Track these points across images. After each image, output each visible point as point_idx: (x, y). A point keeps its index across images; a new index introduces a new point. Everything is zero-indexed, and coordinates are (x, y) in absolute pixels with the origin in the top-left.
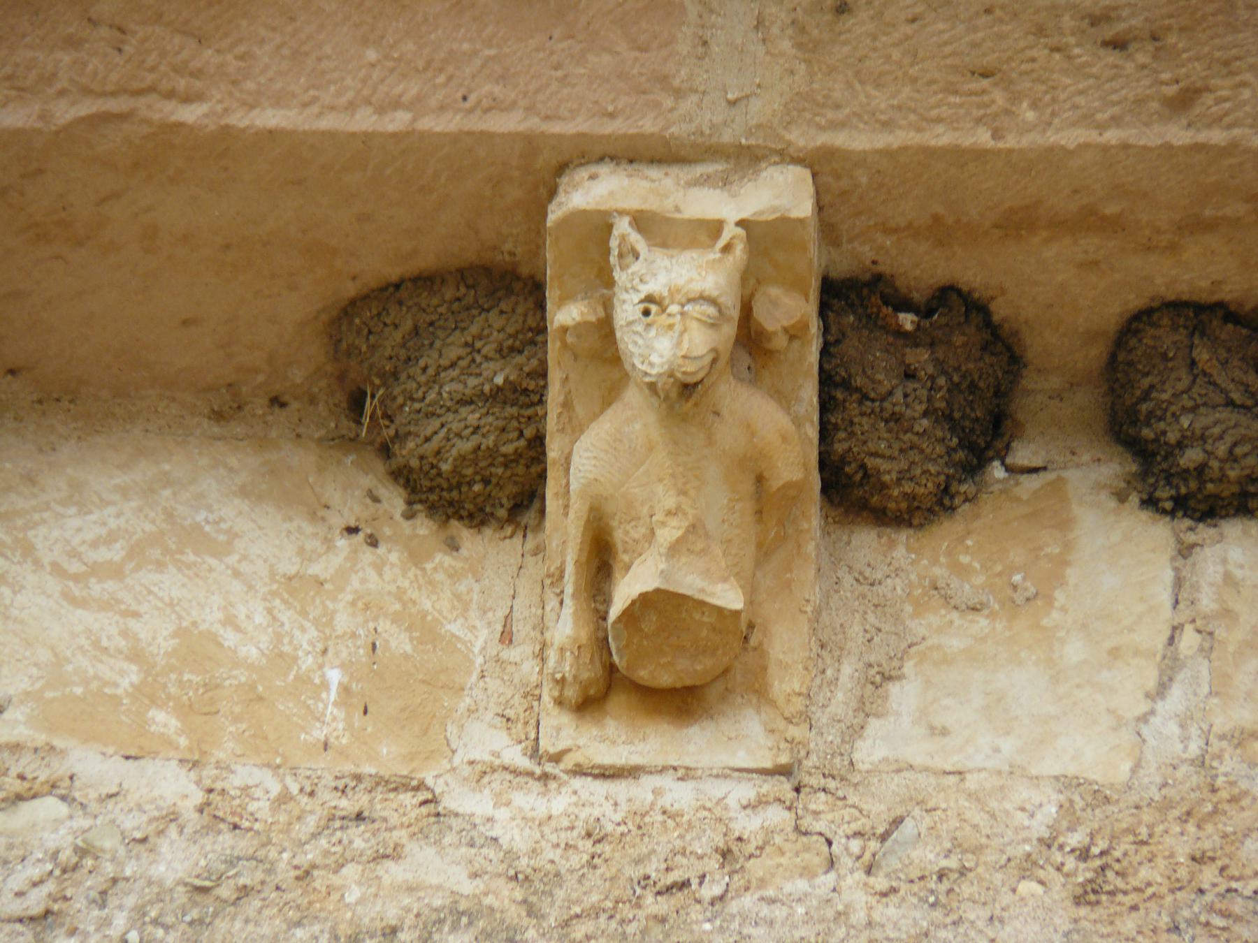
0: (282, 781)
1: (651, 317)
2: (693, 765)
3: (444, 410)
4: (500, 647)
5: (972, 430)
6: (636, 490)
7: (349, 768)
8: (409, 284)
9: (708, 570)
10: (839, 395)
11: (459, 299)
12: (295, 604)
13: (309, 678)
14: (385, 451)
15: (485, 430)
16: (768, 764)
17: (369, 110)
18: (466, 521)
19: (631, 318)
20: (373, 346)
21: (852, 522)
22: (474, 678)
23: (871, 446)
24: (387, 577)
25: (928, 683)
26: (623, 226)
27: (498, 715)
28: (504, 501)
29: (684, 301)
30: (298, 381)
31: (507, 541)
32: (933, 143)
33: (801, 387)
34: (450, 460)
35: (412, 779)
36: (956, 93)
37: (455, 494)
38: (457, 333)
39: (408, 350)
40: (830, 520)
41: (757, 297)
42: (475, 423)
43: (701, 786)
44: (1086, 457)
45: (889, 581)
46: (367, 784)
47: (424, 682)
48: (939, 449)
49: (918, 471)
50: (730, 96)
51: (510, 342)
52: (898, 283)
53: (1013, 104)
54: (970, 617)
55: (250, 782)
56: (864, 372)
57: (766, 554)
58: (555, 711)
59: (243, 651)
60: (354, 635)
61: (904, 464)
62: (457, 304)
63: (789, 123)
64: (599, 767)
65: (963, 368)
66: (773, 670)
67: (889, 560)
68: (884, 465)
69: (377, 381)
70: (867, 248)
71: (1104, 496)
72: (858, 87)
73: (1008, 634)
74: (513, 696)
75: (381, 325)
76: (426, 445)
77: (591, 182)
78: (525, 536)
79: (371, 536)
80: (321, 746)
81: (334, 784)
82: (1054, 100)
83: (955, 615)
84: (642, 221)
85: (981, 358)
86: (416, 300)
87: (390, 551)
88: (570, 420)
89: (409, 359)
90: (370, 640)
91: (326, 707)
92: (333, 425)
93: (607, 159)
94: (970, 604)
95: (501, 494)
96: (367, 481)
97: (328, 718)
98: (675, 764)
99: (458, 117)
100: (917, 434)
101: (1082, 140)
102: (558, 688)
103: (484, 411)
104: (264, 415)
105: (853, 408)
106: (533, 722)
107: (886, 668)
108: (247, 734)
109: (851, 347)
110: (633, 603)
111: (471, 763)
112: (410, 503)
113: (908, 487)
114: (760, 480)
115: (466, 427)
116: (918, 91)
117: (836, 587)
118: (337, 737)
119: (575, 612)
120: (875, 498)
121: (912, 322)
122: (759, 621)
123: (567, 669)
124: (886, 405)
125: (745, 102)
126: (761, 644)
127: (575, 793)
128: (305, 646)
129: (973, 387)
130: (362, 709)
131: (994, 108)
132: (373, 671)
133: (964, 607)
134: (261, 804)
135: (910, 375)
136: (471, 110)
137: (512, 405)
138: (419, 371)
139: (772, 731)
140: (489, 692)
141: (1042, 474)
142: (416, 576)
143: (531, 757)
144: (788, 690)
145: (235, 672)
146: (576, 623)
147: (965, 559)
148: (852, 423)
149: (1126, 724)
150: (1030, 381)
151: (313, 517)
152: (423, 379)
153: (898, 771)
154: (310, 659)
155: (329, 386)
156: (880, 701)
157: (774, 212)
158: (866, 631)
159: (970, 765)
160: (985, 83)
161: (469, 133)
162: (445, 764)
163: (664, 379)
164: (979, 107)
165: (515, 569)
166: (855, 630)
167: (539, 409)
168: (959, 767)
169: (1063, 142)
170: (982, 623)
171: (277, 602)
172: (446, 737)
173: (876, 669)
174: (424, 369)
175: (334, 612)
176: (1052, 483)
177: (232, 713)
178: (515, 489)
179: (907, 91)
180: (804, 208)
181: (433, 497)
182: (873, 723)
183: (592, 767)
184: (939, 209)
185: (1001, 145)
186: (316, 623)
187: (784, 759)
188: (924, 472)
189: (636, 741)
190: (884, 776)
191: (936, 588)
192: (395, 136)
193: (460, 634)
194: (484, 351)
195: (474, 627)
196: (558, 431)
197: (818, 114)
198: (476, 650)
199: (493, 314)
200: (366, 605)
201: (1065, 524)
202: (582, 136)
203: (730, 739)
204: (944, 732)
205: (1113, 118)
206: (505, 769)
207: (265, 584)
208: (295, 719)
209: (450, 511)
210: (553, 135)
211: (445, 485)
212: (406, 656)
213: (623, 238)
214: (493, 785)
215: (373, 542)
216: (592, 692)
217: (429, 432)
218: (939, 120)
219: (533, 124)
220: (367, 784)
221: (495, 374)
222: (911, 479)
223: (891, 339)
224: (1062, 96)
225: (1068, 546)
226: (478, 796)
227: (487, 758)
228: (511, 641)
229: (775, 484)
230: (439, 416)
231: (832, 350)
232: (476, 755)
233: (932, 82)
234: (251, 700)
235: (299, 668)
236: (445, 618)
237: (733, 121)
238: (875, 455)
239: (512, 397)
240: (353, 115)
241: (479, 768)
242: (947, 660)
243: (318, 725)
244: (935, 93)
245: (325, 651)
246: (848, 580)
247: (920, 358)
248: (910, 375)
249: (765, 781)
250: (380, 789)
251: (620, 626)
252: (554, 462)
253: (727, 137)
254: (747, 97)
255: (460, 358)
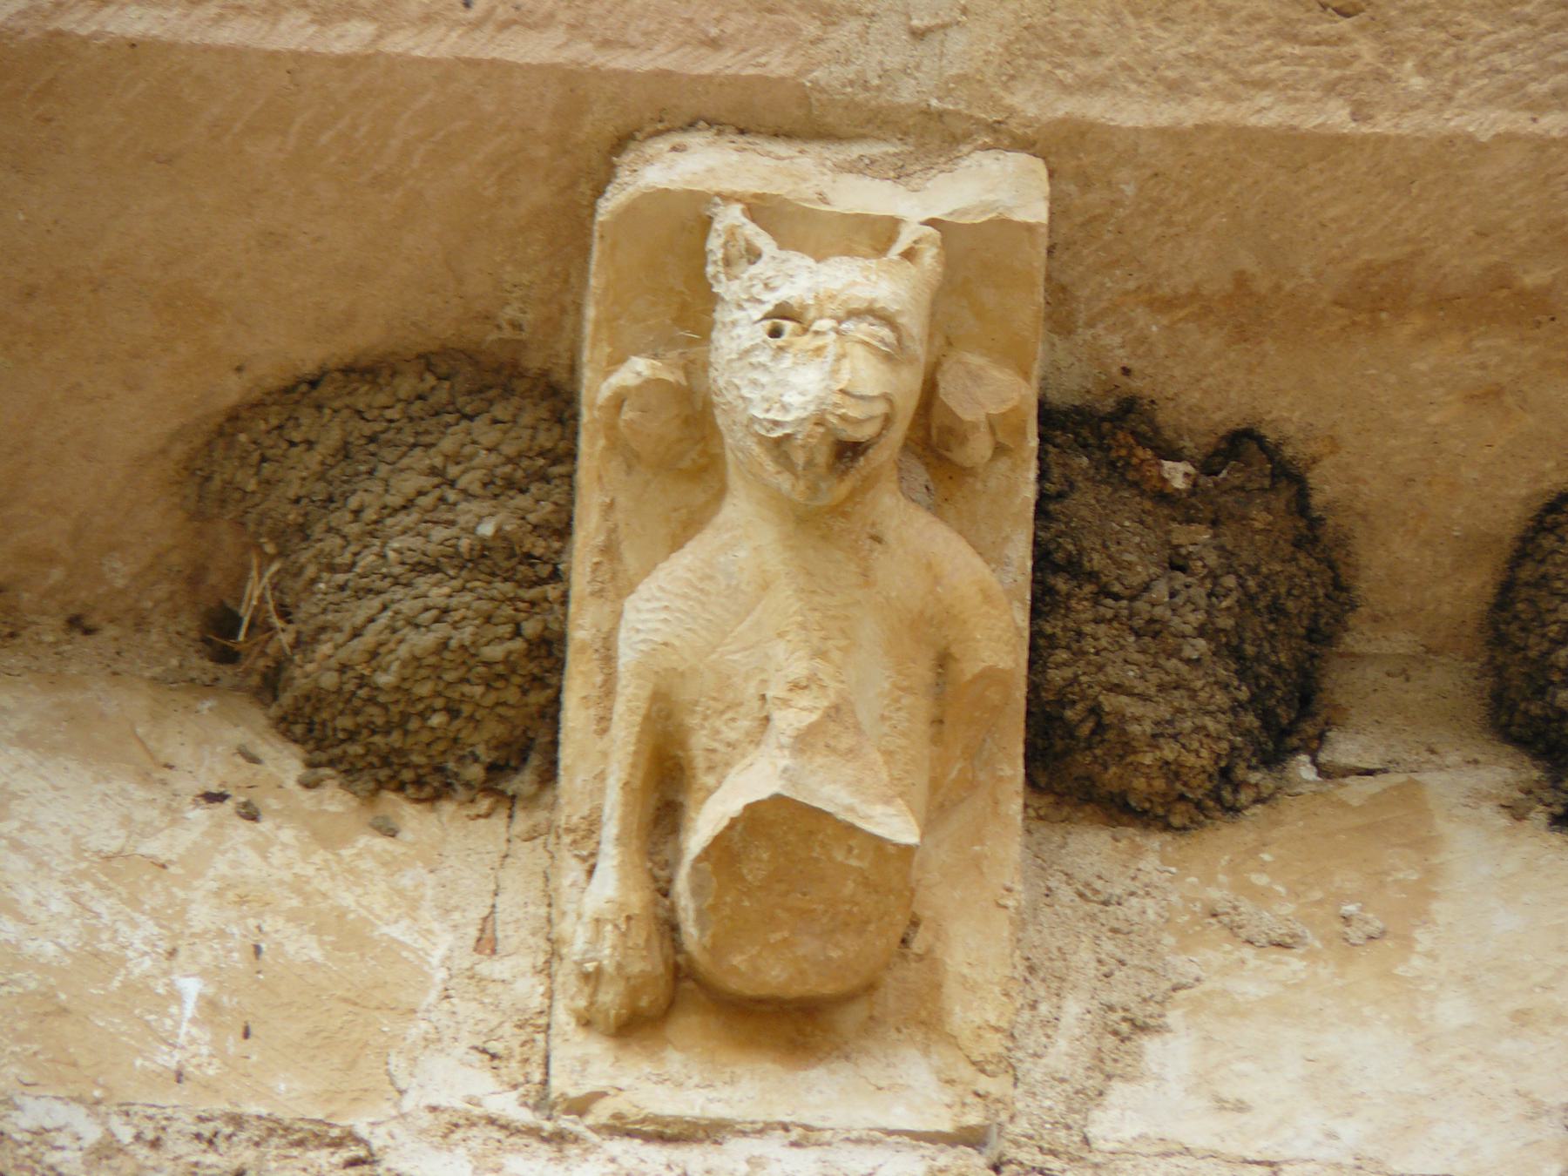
0: (103, 1124)
1: (785, 337)
2: (818, 1124)
3: (388, 581)
4: (477, 957)
5: (1271, 687)
6: (737, 657)
7: (221, 1106)
8: (337, 375)
9: (860, 781)
10: (1061, 584)
11: (421, 397)
12: (120, 889)
13: (148, 987)
14: (270, 686)
15: (456, 616)
16: (947, 1127)
17: (305, 16)
18: (411, 791)
19: (747, 344)
20: (268, 482)
21: (1066, 820)
22: (433, 996)
23: (1113, 674)
24: (275, 861)
25: (1208, 1039)
26: (731, 216)
27: (475, 1048)
28: (481, 750)
29: (841, 313)
30: (120, 583)
31: (482, 821)
32: (1252, 121)
33: (1007, 539)
34: (395, 666)
35: (330, 1125)
36: (1294, 38)
37: (395, 738)
38: (418, 452)
39: (330, 483)
40: (1032, 813)
41: (946, 366)
42: (442, 602)
43: (830, 1157)
44: (1453, 758)
45: (1134, 900)
46: (252, 1132)
47: (346, 1000)
48: (1221, 699)
49: (1188, 725)
50: (915, 23)
51: (508, 469)
52: (1161, 417)
53: (1389, 63)
54: (1274, 957)
55: (48, 1124)
56: (1105, 546)
57: (941, 807)
58: (579, 1036)
59: (31, 947)
60: (222, 934)
61: (1164, 712)
62: (418, 404)
63: (1012, 77)
64: (655, 1119)
65: (1264, 570)
66: (951, 988)
67: (1132, 872)
68: (1133, 707)
69: (270, 549)
70: (1116, 340)
71: (1487, 810)
72: (1131, 21)
73: (1338, 982)
74: (501, 1024)
75: (284, 445)
76: (355, 642)
77: (673, 154)
78: (511, 817)
79: (246, 805)
80: (173, 1076)
81: (194, 1129)
82: (1459, 58)
83: (1248, 952)
84: (761, 209)
85: (1294, 559)
86: (348, 400)
87: (279, 828)
88: (614, 577)
89: (331, 499)
90: (250, 942)
91: (178, 1024)
92: (174, 662)
93: (702, 124)
94: (1275, 936)
95: (475, 739)
96: (238, 735)
97: (182, 1040)
98: (787, 1119)
99: (454, 35)
100: (1188, 661)
101: (1502, 128)
102: (587, 990)
103: (456, 583)
104: (56, 644)
105: (1083, 610)
106: (537, 1058)
107: (1138, 1013)
108: (41, 1057)
109: (1084, 503)
110: (733, 823)
111: (433, 1109)
112: (311, 765)
113: (1169, 751)
114: (943, 661)
115: (427, 609)
116: (1231, 32)
117: (1048, 900)
118: (199, 1066)
119: (622, 865)
120: (1113, 770)
121: (1187, 475)
122: (927, 913)
123: (607, 954)
124: (1140, 605)
125: (939, 36)
126: (930, 950)
127: (613, 1160)
128: (138, 944)
129: (1276, 610)
130: (240, 1031)
131: (1357, 67)
132: (257, 981)
133: (1263, 940)
134: (68, 1154)
135: (1178, 564)
136: (477, 25)
137: (506, 580)
138: (349, 517)
139: (950, 1082)
140: (460, 1018)
141: (1380, 777)
142: (326, 861)
143: (536, 1108)
144: (978, 1021)
145: (17, 975)
146: (623, 879)
147: (1261, 880)
148: (1080, 635)
149: (1548, 1112)
150: (1358, 638)
151: (145, 778)
152: (355, 528)
153: (1166, 1155)
154: (147, 963)
155: (171, 596)
156: (1129, 1060)
157: (984, 212)
158: (1100, 961)
159: (1287, 1153)
160: (1344, 24)
161: (473, 63)
162: (388, 1109)
163: (808, 427)
164: (1334, 63)
165: (496, 858)
166: (1084, 956)
167: (552, 591)
168: (1269, 1156)
169: (1471, 129)
170: (1293, 965)
171: (88, 886)
172: (388, 1073)
173: (1121, 1014)
174: (357, 513)
175: (187, 902)
176: (1398, 787)
177: (14, 1030)
178: (500, 730)
179: (1212, 32)
180: (1036, 212)
181: (355, 749)
182: (1119, 1092)
183: (643, 1121)
184: (1247, 262)
185: (1365, 129)
186: (155, 914)
187: (973, 1118)
188: (1198, 729)
189: (718, 1084)
190: (1143, 1160)
191: (1214, 915)
192: (344, 61)
193: (407, 939)
194: (462, 483)
195: (430, 931)
196: (593, 594)
197: (1060, 66)
198: (435, 961)
199: (480, 424)
200: (240, 897)
201: (1425, 844)
202: (663, 76)
203: (880, 1089)
204: (1241, 1107)
205: (1555, 93)
206: (492, 1121)
207: (67, 862)
208: (124, 1039)
209: (383, 774)
210: (616, 73)
211: (380, 721)
212: (314, 965)
213: (732, 233)
214: (471, 1143)
215: (250, 814)
216: (644, 1002)
217: (360, 619)
218: (1263, 84)
219: (582, 52)
220: (252, 1132)
221: (481, 518)
222: (1175, 737)
223: (1148, 505)
224: (1474, 51)
225: (1431, 873)
226: (445, 1156)
227: (460, 1105)
228: (494, 951)
229: (970, 669)
230: (379, 593)
231: (1052, 507)
232: (441, 1100)
233: (1258, 18)
234: (46, 1014)
235: (129, 973)
236: (379, 917)
237: (917, 67)
238: (1116, 688)
239: (507, 564)
240: (274, 24)
241: (445, 1117)
242: (1239, 1011)
243: (165, 1048)
244: (1260, 37)
245: (172, 953)
246: (1066, 894)
247: (1196, 538)
248: (1178, 564)
249: (942, 1151)
250: (275, 1141)
251: (707, 866)
252: (583, 649)
253: (907, 94)
254: (944, 26)
255: (421, 493)
